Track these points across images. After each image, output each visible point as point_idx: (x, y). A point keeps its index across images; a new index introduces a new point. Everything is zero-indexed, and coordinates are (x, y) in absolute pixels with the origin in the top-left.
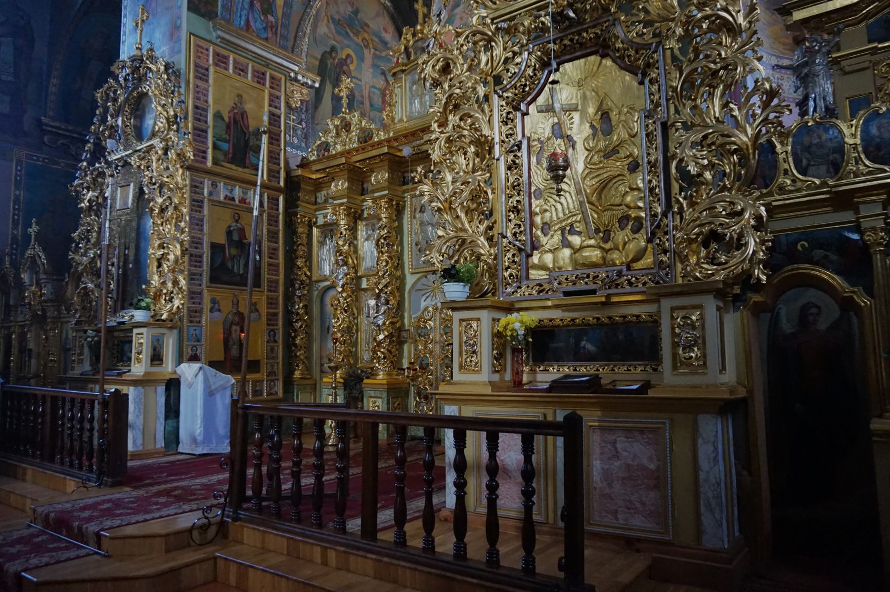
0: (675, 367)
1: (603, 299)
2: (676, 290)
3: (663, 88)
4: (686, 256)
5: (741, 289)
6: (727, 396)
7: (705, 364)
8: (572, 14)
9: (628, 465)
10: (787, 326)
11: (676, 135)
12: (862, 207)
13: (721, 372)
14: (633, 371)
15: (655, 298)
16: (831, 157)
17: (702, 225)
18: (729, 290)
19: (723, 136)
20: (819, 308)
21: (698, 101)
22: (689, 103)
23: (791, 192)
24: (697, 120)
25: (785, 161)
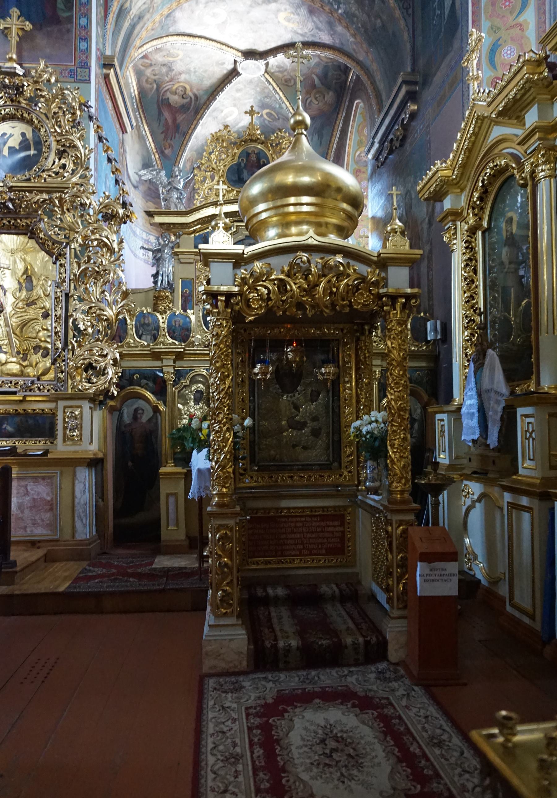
0: (64, 441)
1: (21, 398)
2: (68, 396)
3: (68, 272)
4: (74, 376)
5: (104, 398)
6: (92, 456)
7: (81, 439)
8: (11, 206)
9: (34, 499)
10: (127, 419)
11: (73, 303)
12: (164, 361)
13: (90, 444)
14: (38, 444)
15: (55, 399)
16: (153, 332)
17: (84, 359)
18: (97, 398)
19: (100, 309)
20: (143, 410)
21: (88, 286)
22: (83, 286)
23: (133, 347)
24: (86, 296)
25: (132, 329)
